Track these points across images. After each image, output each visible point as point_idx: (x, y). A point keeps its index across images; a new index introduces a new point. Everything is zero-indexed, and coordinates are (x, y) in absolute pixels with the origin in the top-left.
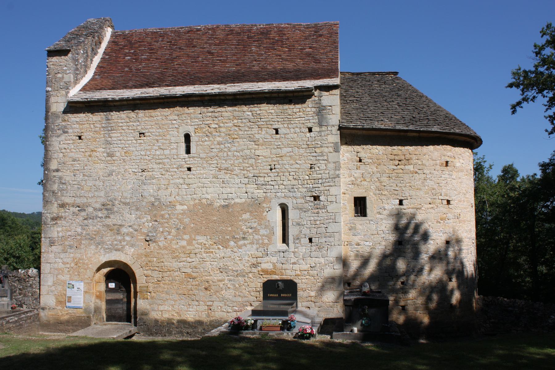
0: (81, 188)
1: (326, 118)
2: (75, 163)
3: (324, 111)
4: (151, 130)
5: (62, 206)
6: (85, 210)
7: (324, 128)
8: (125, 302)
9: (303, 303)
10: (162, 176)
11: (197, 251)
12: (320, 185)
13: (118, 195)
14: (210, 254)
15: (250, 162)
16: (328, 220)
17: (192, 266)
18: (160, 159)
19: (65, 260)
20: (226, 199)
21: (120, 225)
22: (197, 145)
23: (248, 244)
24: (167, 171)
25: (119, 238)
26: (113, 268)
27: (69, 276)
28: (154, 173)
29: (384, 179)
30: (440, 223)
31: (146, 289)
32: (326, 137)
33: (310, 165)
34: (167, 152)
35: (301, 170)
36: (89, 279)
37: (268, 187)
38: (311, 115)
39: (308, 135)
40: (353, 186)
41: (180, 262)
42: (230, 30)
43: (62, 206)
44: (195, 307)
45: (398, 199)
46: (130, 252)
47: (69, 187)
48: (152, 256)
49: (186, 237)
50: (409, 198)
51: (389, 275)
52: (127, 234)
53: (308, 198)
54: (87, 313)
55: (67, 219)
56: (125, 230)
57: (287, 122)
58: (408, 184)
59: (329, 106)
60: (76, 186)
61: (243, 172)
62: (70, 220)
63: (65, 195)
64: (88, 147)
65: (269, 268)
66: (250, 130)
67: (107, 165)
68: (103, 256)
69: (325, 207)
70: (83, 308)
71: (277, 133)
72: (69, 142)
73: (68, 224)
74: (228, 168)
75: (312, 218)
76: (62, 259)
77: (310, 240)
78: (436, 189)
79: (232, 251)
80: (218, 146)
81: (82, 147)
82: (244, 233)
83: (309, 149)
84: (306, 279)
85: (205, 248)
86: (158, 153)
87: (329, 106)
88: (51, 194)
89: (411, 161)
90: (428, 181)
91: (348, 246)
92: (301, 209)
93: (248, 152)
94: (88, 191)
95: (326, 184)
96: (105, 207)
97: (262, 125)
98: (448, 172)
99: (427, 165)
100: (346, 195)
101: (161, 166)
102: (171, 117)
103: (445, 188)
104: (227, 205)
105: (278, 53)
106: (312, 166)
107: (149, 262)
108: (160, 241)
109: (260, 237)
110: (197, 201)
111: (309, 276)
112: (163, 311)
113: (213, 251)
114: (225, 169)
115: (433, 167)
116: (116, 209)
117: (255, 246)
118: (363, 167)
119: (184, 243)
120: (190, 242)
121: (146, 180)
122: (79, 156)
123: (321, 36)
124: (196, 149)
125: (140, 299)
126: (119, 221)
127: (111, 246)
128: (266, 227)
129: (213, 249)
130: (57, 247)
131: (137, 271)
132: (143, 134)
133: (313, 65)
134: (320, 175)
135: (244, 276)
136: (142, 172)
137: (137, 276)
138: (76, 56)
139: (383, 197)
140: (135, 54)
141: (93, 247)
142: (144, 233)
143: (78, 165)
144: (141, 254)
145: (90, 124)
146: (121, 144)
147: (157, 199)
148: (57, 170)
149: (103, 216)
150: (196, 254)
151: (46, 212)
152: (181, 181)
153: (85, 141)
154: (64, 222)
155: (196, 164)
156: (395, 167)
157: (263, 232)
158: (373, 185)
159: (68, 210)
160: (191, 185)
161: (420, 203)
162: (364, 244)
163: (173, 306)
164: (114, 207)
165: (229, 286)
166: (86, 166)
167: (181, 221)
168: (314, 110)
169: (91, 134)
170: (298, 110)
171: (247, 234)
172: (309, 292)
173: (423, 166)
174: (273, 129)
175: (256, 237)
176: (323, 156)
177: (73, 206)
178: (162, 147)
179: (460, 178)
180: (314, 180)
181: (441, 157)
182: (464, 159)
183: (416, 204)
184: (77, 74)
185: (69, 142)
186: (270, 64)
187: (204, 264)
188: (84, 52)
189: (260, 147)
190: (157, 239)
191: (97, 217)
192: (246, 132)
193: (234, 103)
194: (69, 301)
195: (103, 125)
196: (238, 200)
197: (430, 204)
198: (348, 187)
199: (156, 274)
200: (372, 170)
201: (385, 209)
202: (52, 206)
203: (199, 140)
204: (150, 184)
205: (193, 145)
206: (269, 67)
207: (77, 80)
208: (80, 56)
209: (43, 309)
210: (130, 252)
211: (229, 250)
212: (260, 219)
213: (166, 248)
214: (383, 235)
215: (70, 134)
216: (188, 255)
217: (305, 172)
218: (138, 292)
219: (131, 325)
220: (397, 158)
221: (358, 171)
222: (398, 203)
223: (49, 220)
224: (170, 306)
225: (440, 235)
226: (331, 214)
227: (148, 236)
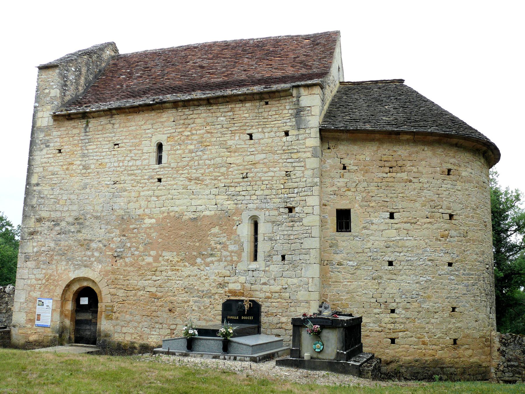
0: (57, 202)
1: (304, 120)
2: (53, 176)
3: (302, 113)
4: (125, 141)
5: (39, 220)
6: (58, 225)
7: (302, 131)
9: (273, 330)
10: (133, 188)
11: (163, 268)
12: (295, 195)
13: (89, 208)
14: (176, 272)
15: (222, 171)
16: (304, 235)
17: (157, 284)
18: (132, 170)
19: (37, 276)
20: (195, 212)
21: (90, 240)
22: (169, 155)
23: (216, 261)
24: (138, 182)
25: (89, 253)
27: (40, 293)
28: (125, 185)
29: (372, 187)
30: (440, 240)
31: (110, 308)
32: (304, 141)
33: (285, 172)
34: (138, 163)
35: (275, 178)
37: (239, 198)
38: (288, 118)
39: (284, 139)
40: (336, 196)
41: (145, 280)
42: (226, 45)
43: (39, 220)
44: (158, 330)
45: (387, 212)
46: (98, 268)
47: (46, 201)
48: (118, 273)
49: (153, 253)
50: (401, 210)
51: (376, 301)
52: (97, 250)
53: (282, 210)
55: (43, 233)
56: (94, 246)
57: (263, 126)
58: (401, 195)
59: (308, 107)
60: (53, 200)
61: (213, 182)
62: (45, 235)
63: (43, 209)
64: (66, 160)
65: (237, 289)
66: (223, 135)
67: (83, 178)
68: (72, 272)
69: (300, 220)
71: (251, 138)
72: (50, 156)
73: (43, 240)
74: (198, 178)
75: (286, 233)
76: (35, 275)
77: (283, 257)
78: (435, 201)
79: (199, 269)
80: (189, 155)
81: (61, 160)
82: (213, 249)
83: (285, 154)
84: (277, 302)
85: (171, 265)
86: (130, 164)
87: (308, 107)
88: (30, 208)
89: (404, 168)
90: (425, 191)
91: (328, 266)
92: (273, 222)
93: (219, 160)
94: (63, 205)
95: (303, 194)
96: (77, 221)
97: (236, 130)
98: (451, 182)
99: (424, 172)
100: (327, 207)
101: (133, 177)
102: (145, 127)
103: (447, 199)
104: (195, 218)
105: (270, 63)
106: (287, 173)
107: (116, 279)
108: (127, 257)
109: (229, 254)
110: (166, 214)
111: (281, 298)
112: (126, 334)
113: (179, 268)
114: (196, 179)
115: (432, 175)
116: (88, 223)
117: (223, 264)
118: (347, 175)
119: (150, 260)
120: (156, 260)
121: (117, 192)
122: (57, 169)
123: (318, 44)
124: (168, 158)
126: (89, 236)
127: (80, 262)
128: (235, 242)
129: (179, 266)
130: (32, 262)
132: (118, 144)
133: (303, 71)
134: (296, 184)
135: (210, 297)
136: (114, 184)
138: (66, 72)
139: (370, 210)
140: (129, 73)
141: (64, 263)
142: (112, 249)
143: (56, 179)
145: (69, 137)
146: (97, 156)
147: (126, 212)
148: (38, 185)
149: (75, 230)
150: (161, 271)
151: (24, 227)
152: (151, 193)
153: (64, 154)
154: (39, 237)
155: (166, 174)
156: (385, 175)
157: (231, 248)
158: (359, 196)
159: (43, 225)
160: (160, 198)
161: (415, 217)
162: (347, 264)
163: (136, 328)
164: (86, 221)
165: (194, 308)
166: (63, 179)
167: (149, 235)
168: (291, 111)
169: (70, 147)
170: (274, 113)
171: (216, 250)
172: (280, 318)
173: (419, 174)
174: (247, 134)
175: (225, 253)
176: (299, 162)
177: (48, 220)
178: (133, 158)
179: (467, 190)
180: (289, 189)
181: (442, 164)
182: (472, 168)
183: (410, 218)
184: (65, 90)
185: (50, 156)
186: (258, 73)
187: (169, 283)
188: (76, 70)
189: (233, 154)
190: (124, 255)
191: (69, 231)
192: (218, 139)
193: (208, 108)
194: (38, 319)
195: (82, 138)
196: (207, 213)
197: (427, 218)
198: (330, 198)
199: (121, 293)
200: (358, 178)
201: (372, 224)
202: (30, 220)
203: (171, 149)
204: (121, 197)
205: (164, 154)
206: (256, 75)
207: (65, 96)
208: (70, 73)
209: (14, 326)
210: (98, 268)
211: (196, 267)
212: (231, 233)
213: (132, 265)
214: (370, 254)
215: (51, 148)
216: (154, 273)
217: (279, 180)
220: (387, 164)
221: (341, 180)
222: (389, 216)
223: (27, 234)
224: (134, 328)
225: (441, 255)
226: (307, 228)
227: (116, 251)
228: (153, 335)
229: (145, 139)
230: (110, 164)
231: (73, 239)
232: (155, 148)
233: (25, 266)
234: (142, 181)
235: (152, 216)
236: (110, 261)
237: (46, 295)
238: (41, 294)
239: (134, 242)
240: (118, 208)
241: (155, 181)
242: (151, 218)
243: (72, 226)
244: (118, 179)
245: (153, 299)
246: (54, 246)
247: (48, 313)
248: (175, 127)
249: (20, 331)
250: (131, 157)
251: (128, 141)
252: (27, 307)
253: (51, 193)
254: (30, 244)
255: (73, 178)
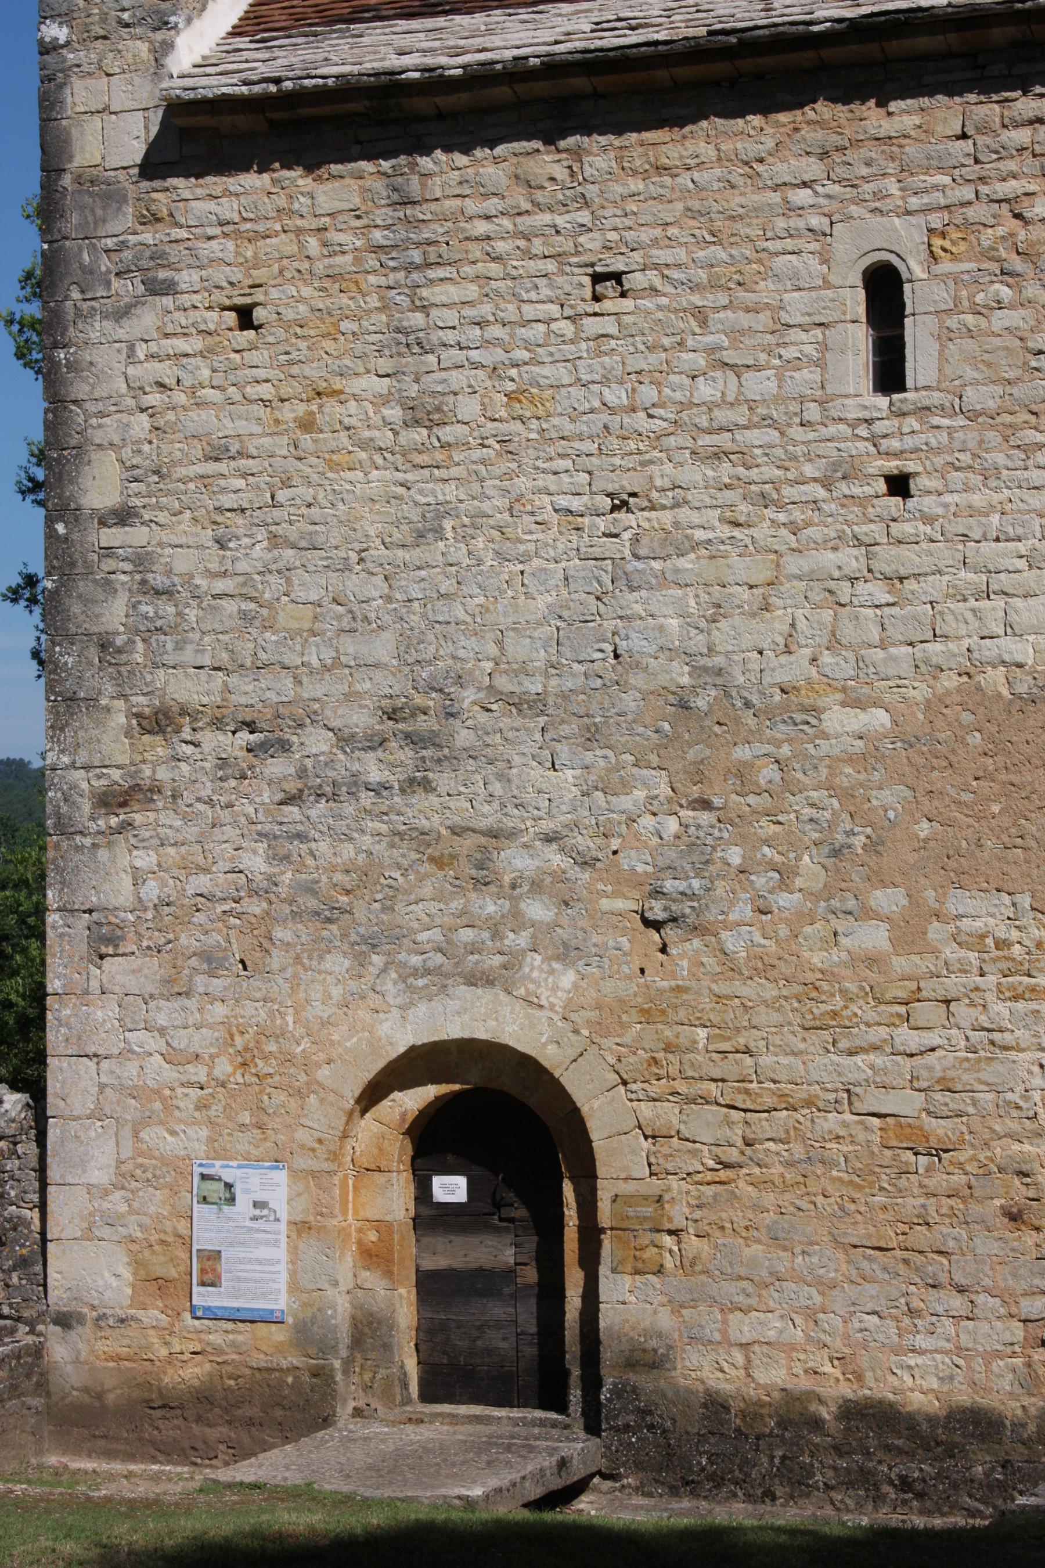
2: (222, 467)
4: (663, 255)
6: (285, 747)
8: (527, 1286)
10: (737, 533)
11: (954, 984)
17: (924, 1074)
19: (181, 1039)
21: (494, 834)
22: (946, 336)
25: (490, 907)
26: (457, 1087)
28: (684, 514)
36: (321, 1151)
41: (851, 1053)
44: (948, 1326)
46: (555, 989)
47: (192, 614)
52: (536, 886)
54: (312, 1351)
55: (188, 797)
60: (230, 607)
64: (295, 370)
67: (410, 477)
68: (395, 1013)
70: (290, 1320)
72: (181, 345)
73: (192, 832)
76: (162, 1031)
81: (261, 373)
85: (1004, 965)
88: (93, 654)
94: (299, 632)
101: (726, 470)
102: (782, 170)
108: (729, 927)
110: (950, 681)
112: (756, 1348)
116: (464, 737)
121: (636, 557)
122: (242, 426)
125: (614, 1271)
127: (439, 958)
131: (596, 1104)
132: (617, 277)
136: (614, 508)
137: (594, 1136)
141: (338, 963)
142: (635, 881)
143: (240, 483)
144: (621, 1001)
145: (299, 231)
146: (487, 343)
147: (705, 670)
148: (123, 516)
151: (66, 759)
152: (851, 559)
154: (168, 818)
155: (938, 451)
160: (911, 585)
163: (811, 1315)
166: (287, 484)
169: (307, 291)
177: (218, 724)
185: (181, 345)
187: (996, 1066)
191: (356, 784)
204: (663, 581)
209: (65, 1321)
210: (555, 989)
213: (764, 968)
215: (186, 300)
216: (902, 1010)
218: (603, 1231)
219: (567, 1427)
223: (87, 807)
227: (657, 893)
228: (921, 1352)
229: (789, 244)
230: (575, 391)
231: (384, 828)
232: (857, 302)
233: (94, 984)
234: (789, 492)
235: (866, 690)
236: (626, 945)
237: (243, 1142)
238: (211, 1140)
239: (767, 842)
240: (652, 650)
241: (868, 490)
242: (859, 704)
243: (371, 756)
244: (628, 482)
245: (909, 1155)
246: (264, 868)
247: (267, 1243)
248: (972, 171)
249: (101, 1346)
250: (711, 350)
251: (681, 254)
252: (132, 1211)
253: (214, 567)
254: (113, 860)
255: (349, 475)
